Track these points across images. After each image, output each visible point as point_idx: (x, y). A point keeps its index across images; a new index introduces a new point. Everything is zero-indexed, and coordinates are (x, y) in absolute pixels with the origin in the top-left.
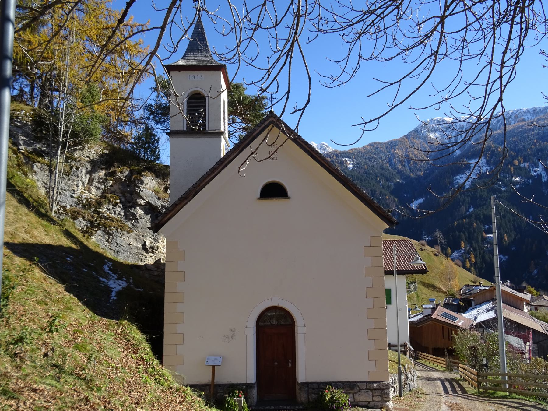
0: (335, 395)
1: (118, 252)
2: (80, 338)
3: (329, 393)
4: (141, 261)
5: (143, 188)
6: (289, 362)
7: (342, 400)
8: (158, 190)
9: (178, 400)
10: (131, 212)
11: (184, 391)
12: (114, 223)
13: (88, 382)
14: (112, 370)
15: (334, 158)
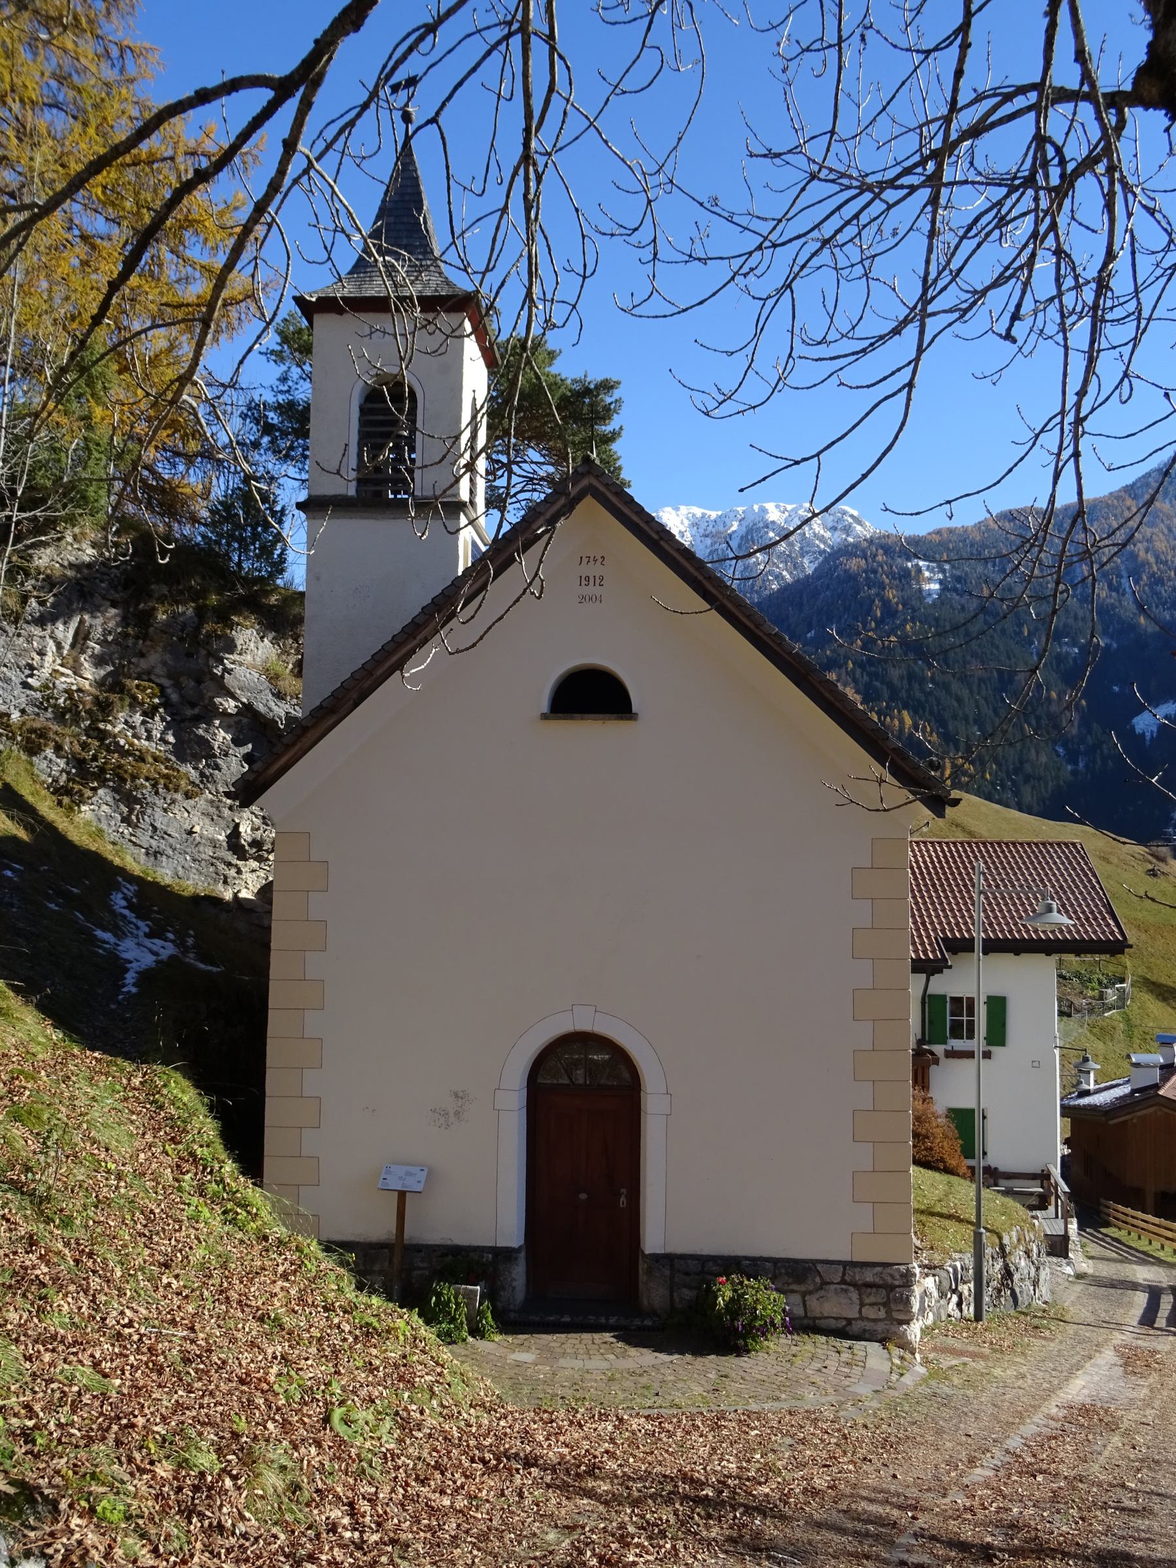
0: (745, 1293)
1: (157, 854)
2: (27, 1093)
3: (729, 1286)
4: (225, 882)
5: (233, 663)
6: (620, 1195)
7: (764, 1309)
8: (279, 669)
9: (281, 1269)
10: (197, 735)
11: (299, 1249)
12: (145, 768)
13: (40, 1202)
14: (107, 1179)
15: (879, 558)
